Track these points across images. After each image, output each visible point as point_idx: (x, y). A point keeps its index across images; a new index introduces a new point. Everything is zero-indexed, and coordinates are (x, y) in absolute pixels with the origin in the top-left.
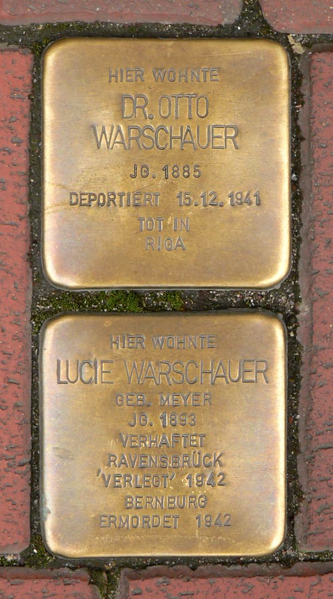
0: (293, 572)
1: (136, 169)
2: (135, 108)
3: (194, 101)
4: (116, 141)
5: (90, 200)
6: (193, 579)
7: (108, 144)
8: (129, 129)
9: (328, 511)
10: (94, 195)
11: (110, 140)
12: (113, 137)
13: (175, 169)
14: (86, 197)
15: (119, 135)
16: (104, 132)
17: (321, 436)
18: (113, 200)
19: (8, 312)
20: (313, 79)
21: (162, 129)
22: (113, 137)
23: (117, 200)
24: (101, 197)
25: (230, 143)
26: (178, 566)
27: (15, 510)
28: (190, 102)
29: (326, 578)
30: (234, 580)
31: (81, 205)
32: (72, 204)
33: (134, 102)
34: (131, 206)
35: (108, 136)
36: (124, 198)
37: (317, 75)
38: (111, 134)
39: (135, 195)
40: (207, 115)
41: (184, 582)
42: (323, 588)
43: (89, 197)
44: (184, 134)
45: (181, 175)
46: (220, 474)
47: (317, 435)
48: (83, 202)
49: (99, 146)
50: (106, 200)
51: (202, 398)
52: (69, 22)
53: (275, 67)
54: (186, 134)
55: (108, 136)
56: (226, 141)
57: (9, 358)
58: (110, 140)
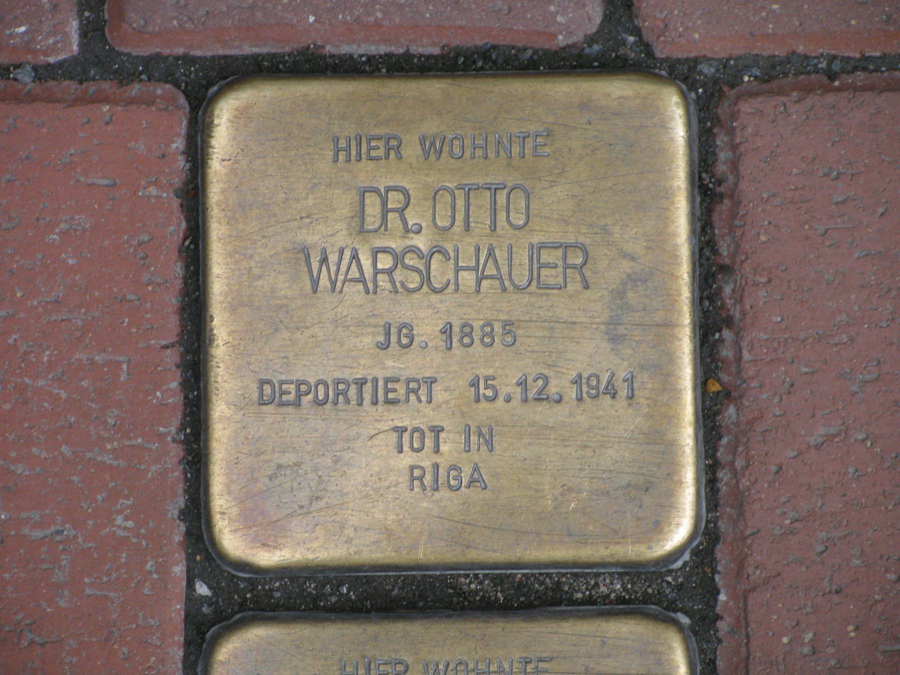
0: (219, 405)
1: (388, 334)
2: (385, 211)
3: (502, 198)
4: (348, 277)
5: (299, 395)
7: (334, 284)
8: (375, 253)
11: (337, 274)
12: (343, 268)
13: (487, 340)
14: (292, 388)
16: (324, 260)
18: (345, 393)
20: (742, 148)
21: (438, 251)
22: (343, 268)
23: (353, 391)
24: (321, 389)
26: (181, 502)
31: (282, 404)
32: (262, 403)
33: (384, 203)
34: (380, 403)
35: (333, 269)
36: (368, 389)
37: (747, 141)
39: (386, 383)
40: (526, 224)
43: (298, 389)
44: (482, 261)
45: (477, 342)
48: (285, 398)
49: (315, 283)
50: (331, 393)
52: (284, 53)
53: (664, 126)
55: (333, 269)
56: (565, 274)
58: (337, 274)
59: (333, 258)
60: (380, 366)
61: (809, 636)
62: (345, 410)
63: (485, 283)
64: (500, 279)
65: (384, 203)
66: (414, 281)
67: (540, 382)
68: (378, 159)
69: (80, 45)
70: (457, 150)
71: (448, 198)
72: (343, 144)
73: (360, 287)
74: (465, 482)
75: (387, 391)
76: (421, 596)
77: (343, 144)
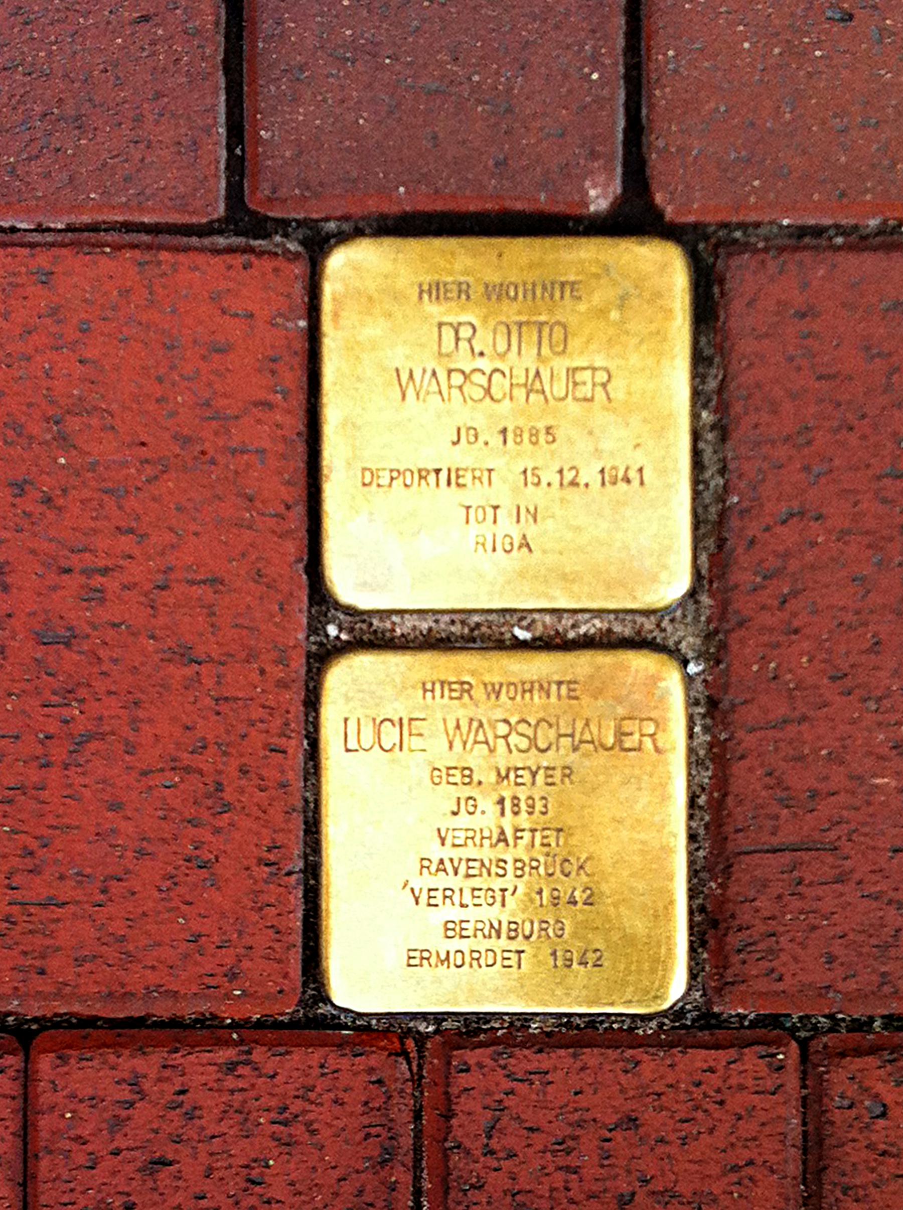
3: (546, 331)
6: (547, 1050)
9: (753, 948)
10: (398, 471)
15: (481, 731)
17: (741, 834)
19: (270, 647)
25: (599, 392)
27: (280, 941)
28: (540, 332)
29: (895, 255)
30: (610, 1051)
36: (443, 476)
38: (422, 381)
41: (536, 1053)
42: (746, 1067)
44: (530, 381)
46: (572, 468)
47: (738, 831)
51: (565, 887)
54: (534, 381)
57: (271, 715)
59: (417, 375)
60: (308, 851)
61: (772, 665)
62: (531, 1073)
63: (532, 396)
64: (543, 392)
65: (457, 332)
66: (479, 393)
67: (573, 472)
68: (451, 299)
69: (227, 210)
70: (512, 294)
71: (505, 330)
72: (429, 686)
73: (439, 397)
74: (516, 545)
75: (458, 477)
76: (691, 1074)
77: (429, 686)
